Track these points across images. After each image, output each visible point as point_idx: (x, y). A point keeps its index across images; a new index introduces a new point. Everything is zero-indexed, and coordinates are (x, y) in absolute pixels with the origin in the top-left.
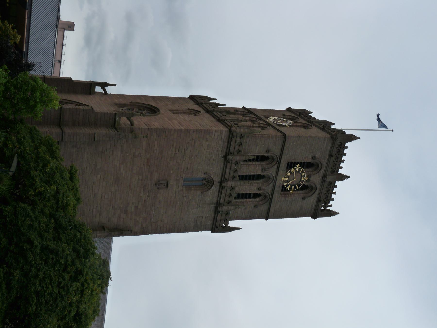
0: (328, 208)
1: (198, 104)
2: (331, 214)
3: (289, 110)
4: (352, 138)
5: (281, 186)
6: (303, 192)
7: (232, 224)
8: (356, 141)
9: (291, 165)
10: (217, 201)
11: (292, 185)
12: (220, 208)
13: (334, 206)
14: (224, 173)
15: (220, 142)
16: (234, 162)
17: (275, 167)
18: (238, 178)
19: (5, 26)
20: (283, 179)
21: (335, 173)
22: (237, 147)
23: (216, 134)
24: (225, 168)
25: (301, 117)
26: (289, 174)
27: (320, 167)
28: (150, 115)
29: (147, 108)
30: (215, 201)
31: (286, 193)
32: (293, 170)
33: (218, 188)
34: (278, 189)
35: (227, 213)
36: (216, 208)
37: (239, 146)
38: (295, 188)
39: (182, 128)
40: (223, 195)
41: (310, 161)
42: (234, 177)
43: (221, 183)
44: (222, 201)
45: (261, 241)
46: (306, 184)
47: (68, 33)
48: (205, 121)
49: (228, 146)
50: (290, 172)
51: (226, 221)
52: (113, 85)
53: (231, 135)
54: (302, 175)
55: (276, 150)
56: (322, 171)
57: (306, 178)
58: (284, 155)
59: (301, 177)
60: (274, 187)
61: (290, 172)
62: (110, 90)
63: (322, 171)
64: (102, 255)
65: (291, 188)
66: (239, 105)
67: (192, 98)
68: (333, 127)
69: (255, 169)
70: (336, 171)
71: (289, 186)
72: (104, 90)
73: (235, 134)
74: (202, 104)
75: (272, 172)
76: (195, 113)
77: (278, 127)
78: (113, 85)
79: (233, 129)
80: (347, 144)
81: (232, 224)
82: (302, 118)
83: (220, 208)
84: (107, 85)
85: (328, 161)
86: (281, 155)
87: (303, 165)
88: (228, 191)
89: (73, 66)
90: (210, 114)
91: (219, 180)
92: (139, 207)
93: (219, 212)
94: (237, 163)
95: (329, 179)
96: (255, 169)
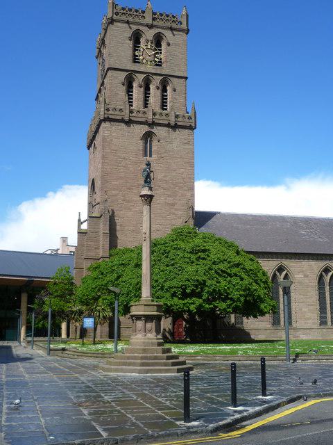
14: (141, 123)
18: (146, 109)
26: (144, 61)
28: (32, 279)
41: (142, 89)
53: (107, 119)
56: (141, 28)
58: (126, 68)
60: (156, 74)
62: (84, 216)
63: (141, 28)
69: (137, 92)
71: (156, 59)
73: (106, 116)
75: (141, 77)
79: (102, 118)
84: (79, 220)
89: (73, 240)
92: (169, 193)
94: (131, 112)
96: (137, 92)
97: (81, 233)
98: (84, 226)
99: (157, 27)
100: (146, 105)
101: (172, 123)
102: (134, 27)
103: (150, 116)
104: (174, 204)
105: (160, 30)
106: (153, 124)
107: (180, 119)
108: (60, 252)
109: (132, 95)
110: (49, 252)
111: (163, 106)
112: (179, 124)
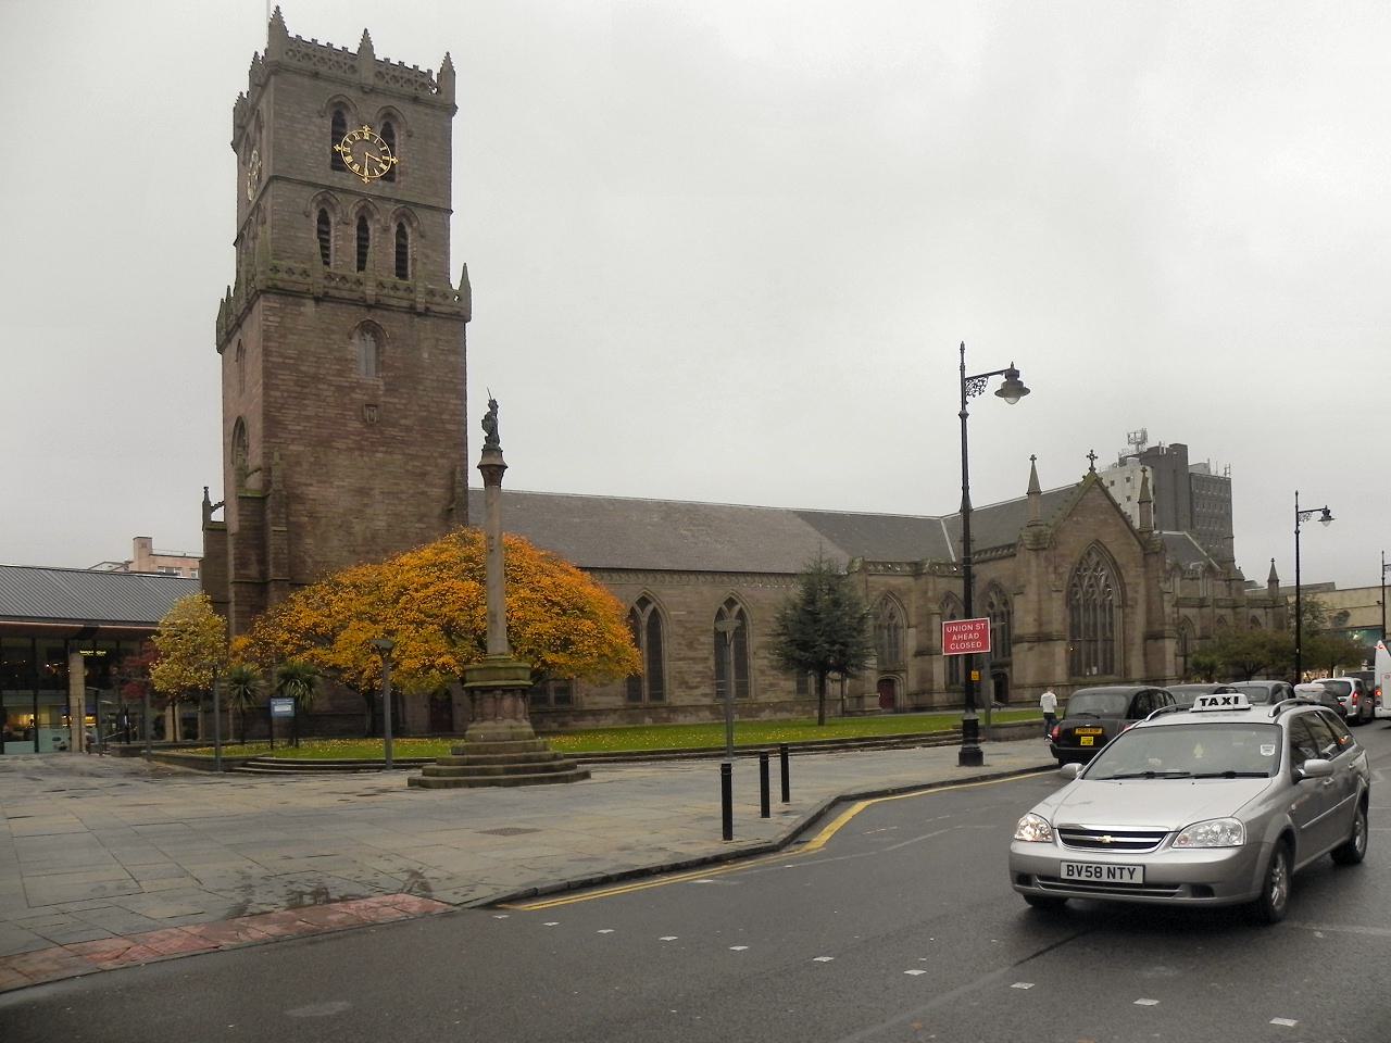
0: (435, 78)
1: (229, 341)
2: (448, 71)
3: (235, 146)
4: (277, 25)
5: (381, 183)
6: (397, 135)
7: (456, 284)
9: (337, 163)
10: (406, 313)
13: (431, 64)
14: (353, 302)
15: (288, 311)
16: (326, 283)
20: (366, 180)
21: (356, 64)
23: (271, 318)
25: (246, 115)
27: (344, 99)
29: (240, 436)
30: (406, 317)
31: (397, 171)
32: (348, 159)
33: (379, 312)
34: (387, 189)
35: (431, 293)
36: (419, 314)
37: (293, 273)
38: (385, 153)
39: (261, 382)
40: (394, 302)
41: (328, 122)
43: (370, 307)
44: (405, 303)
45: (491, 229)
46: (379, 129)
47: (157, 548)
48: (252, 333)
50: (351, 164)
51: (447, 293)
52: (206, 492)
54: (357, 138)
56: (352, 94)
57: (366, 128)
59: (362, 140)
61: (351, 164)
62: (217, 496)
64: (129, 658)
65: (386, 163)
66: (231, 253)
67: (220, 349)
68: (261, 54)
69: (343, 241)
70: (349, 62)
72: (217, 506)
74: (228, 334)
76: (240, 349)
77: (262, 187)
78: (206, 492)
80: (292, 34)
81: (456, 284)
82: (248, 125)
83: (420, 308)
84: (206, 503)
85: (328, 79)
86: (315, 185)
87: (337, 137)
90: (244, 319)
91: (363, 310)
93: (427, 309)
95: (369, 78)
96: (343, 241)
97: (212, 531)
98: (218, 516)
99: (384, 93)
100: (361, 266)
101: (420, 308)
102: (383, 102)
103: (370, 291)
104: (424, 474)
105: (393, 102)
106: (377, 305)
107: (438, 299)
108: (132, 568)
109: (328, 241)
110: (105, 568)
111: (401, 271)
112: (435, 308)
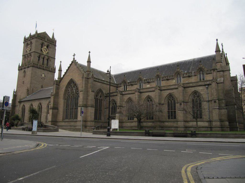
8: (38, 31)
9: (41, 50)
11: (46, 51)
12: (50, 71)
17: (50, 58)
19: (111, 101)
22: (42, 67)
24: (41, 69)
42: (43, 66)
49: (36, 67)
55: (38, 55)
56: (44, 42)
69: (41, 60)
83: (50, 71)
87: (42, 47)
88: (41, 66)
96: (41, 60)
